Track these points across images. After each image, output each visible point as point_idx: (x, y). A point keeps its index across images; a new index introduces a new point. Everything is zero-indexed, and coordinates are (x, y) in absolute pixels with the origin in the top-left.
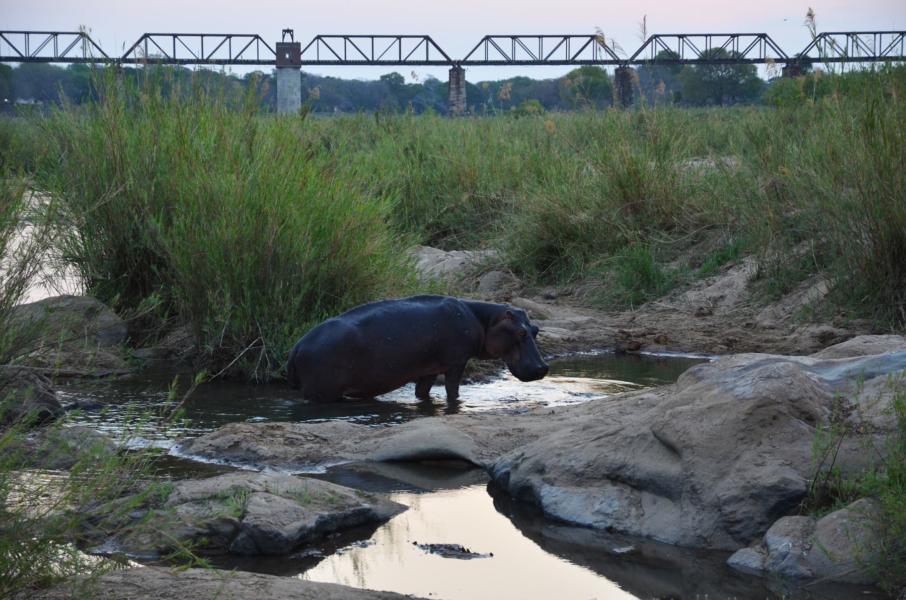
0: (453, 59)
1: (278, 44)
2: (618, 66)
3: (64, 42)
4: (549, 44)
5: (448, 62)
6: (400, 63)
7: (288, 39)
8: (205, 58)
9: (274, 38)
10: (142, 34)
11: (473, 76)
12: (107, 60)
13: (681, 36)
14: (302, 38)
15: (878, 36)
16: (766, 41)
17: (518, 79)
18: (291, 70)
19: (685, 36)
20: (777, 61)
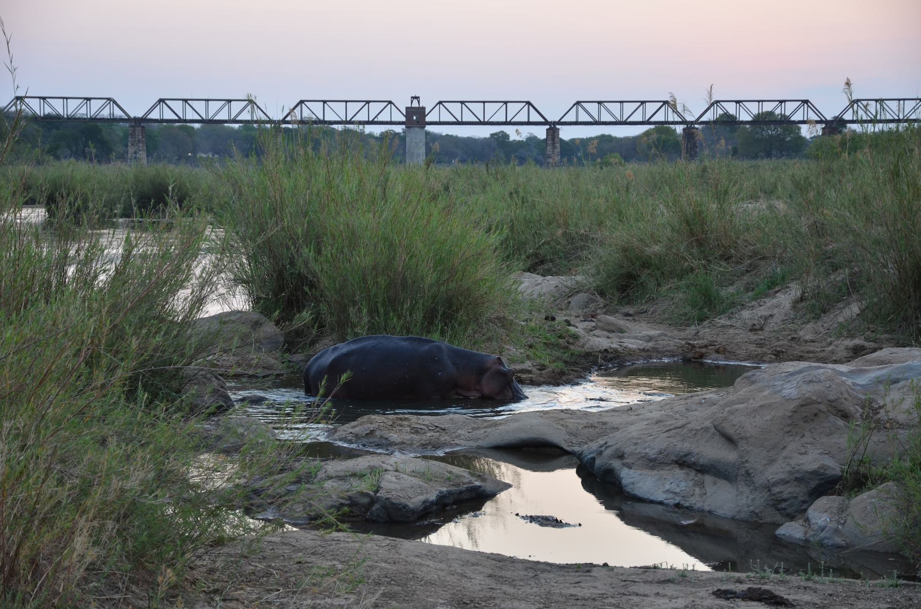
0: (549, 120)
1: (407, 108)
2: (548, 127)
3: (236, 107)
4: (629, 108)
5: (546, 123)
6: (506, 123)
7: (415, 104)
8: (348, 119)
9: (404, 103)
10: (298, 101)
11: (566, 134)
12: (270, 121)
13: (737, 102)
14: (427, 103)
15: (902, 102)
16: (808, 106)
17: (603, 136)
18: (417, 129)
19: (741, 101)
20: (817, 122)
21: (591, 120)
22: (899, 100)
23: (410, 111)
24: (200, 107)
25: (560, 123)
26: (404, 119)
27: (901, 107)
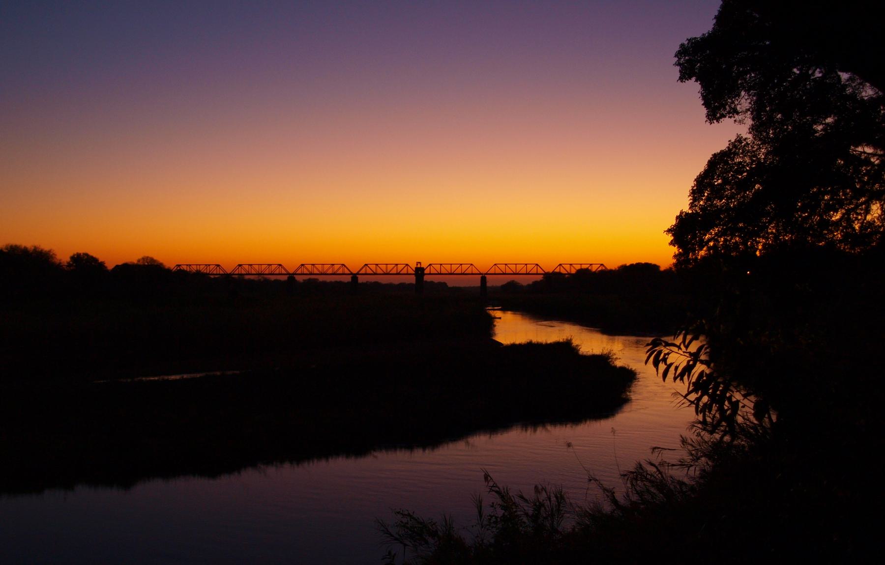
5: (352, 274)
7: (419, 266)
9: (414, 266)
16: (220, 268)
21: (372, 272)
22: (197, 265)
23: (417, 268)
24: (195, 267)
25: (487, 274)
26: (414, 273)
27: (260, 267)
